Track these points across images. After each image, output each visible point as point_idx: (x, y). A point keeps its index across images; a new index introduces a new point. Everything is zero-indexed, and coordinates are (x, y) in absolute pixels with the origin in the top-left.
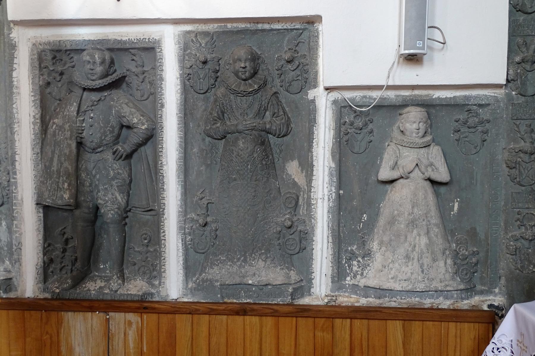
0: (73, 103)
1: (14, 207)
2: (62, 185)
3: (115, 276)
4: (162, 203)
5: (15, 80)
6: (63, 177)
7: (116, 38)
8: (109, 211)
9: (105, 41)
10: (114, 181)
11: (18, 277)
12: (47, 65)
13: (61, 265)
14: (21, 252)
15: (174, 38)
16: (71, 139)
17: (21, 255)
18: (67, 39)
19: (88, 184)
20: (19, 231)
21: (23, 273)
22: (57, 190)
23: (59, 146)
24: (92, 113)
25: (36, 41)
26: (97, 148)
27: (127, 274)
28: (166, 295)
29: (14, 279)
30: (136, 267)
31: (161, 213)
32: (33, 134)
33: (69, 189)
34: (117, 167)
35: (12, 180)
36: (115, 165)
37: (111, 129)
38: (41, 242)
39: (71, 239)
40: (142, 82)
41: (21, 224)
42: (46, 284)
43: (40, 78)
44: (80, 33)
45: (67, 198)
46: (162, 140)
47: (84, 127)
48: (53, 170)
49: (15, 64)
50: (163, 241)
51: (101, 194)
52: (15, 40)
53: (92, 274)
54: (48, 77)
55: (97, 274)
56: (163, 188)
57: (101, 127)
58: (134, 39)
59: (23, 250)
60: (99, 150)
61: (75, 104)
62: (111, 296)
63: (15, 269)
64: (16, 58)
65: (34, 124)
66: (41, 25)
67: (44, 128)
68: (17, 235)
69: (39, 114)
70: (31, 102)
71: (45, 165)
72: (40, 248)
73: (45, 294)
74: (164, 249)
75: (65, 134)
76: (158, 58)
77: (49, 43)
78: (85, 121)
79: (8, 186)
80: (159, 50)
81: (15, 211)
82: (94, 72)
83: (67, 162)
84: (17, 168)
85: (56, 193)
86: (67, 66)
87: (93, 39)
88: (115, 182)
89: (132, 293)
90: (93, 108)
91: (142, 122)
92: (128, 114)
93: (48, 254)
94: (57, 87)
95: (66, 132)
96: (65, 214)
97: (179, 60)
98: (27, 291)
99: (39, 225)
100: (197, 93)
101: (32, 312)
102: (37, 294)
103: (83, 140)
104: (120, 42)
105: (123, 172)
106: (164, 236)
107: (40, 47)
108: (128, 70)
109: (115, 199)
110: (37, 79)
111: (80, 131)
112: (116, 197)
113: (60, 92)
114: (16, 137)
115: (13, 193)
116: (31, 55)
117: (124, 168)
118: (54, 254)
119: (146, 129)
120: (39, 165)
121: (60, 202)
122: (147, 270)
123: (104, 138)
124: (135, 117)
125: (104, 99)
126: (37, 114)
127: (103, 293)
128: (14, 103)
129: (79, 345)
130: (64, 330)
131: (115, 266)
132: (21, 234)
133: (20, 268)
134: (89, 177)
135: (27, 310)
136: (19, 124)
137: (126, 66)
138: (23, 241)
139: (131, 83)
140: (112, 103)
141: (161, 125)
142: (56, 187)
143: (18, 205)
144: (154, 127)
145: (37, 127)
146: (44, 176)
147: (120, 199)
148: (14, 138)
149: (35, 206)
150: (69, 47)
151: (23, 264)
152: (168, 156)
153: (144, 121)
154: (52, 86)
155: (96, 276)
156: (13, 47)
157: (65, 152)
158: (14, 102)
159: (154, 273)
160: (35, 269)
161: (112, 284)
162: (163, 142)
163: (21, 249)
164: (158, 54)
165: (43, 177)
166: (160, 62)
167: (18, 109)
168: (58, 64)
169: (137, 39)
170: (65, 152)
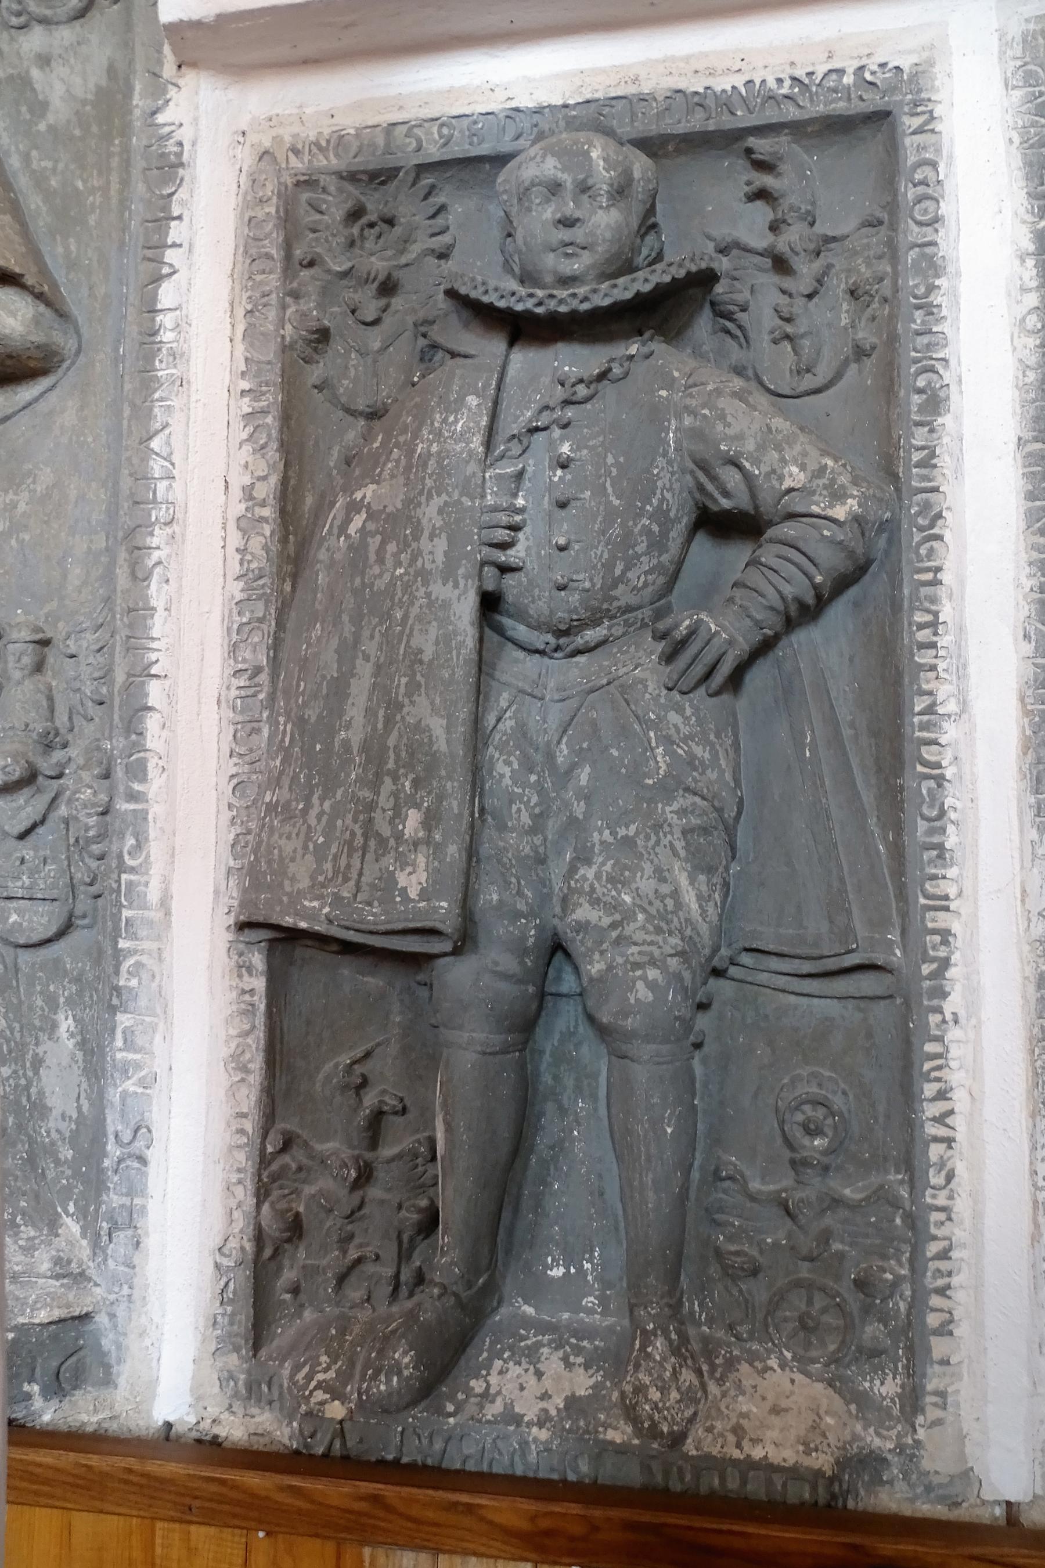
0: (461, 400)
1: (122, 944)
2: (391, 822)
3: (659, 1343)
4: (934, 932)
5: (166, 320)
6: (395, 779)
7: (682, 85)
8: (636, 966)
9: (620, 105)
10: (669, 800)
11: (121, 1311)
13: (345, 1252)
14: (145, 1175)
15: (1002, 53)
17: (143, 1193)
19: (526, 819)
20: (138, 1066)
21: (147, 1286)
22: (365, 849)
24: (562, 439)
25: (277, 139)
26: (584, 624)
27: (699, 1324)
28: (954, 1469)
29: (102, 1319)
30: (759, 1292)
31: (926, 984)
32: (237, 579)
34: (685, 730)
35: (123, 806)
36: (673, 717)
37: (655, 528)
38: (248, 1126)
39: (396, 1113)
40: (810, 296)
41: (154, 1028)
42: (263, 1353)
43: (284, 307)
45: (413, 894)
46: (936, 583)
47: (521, 511)
48: (346, 744)
49: (175, 245)
50: (935, 1151)
51: (598, 876)
52: (177, 136)
53: (504, 1310)
54: (320, 306)
55: (529, 1310)
56: (940, 847)
57: (611, 515)
58: (780, 81)
59: (152, 1169)
60: (591, 635)
61: (472, 400)
62: (646, 1468)
63: (111, 1263)
64: (179, 218)
65: (246, 525)
67: (291, 548)
68: (130, 1086)
69: (274, 480)
70: (237, 424)
71: (301, 722)
72: (241, 1157)
73: (254, 1411)
74: (944, 1193)
76: (912, 160)
77: (339, 141)
78: (527, 484)
79: (102, 836)
80: (916, 122)
81: (127, 964)
82: (578, 234)
84: (149, 745)
85: (356, 862)
86: (415, 250)
87: (560, 102)
88: (675, 806)
89: (776, 1456)
90: (570, 413)
91: (833, 481)
92: (750, 446)
93: (276, 1193)
94: (362, 354)
95: (425, 543)
96: (374, 982)
97: (1028, 164)
98: (162, 1388)
99: (247, 1034)
100: (49, 941)
101: (200, 1533)
102: (213, 1411)
103: (510, 580)
104: (696, 101)
105: (715, 756)
106: (940, 1120)
107: (295, 162)
108: (723, 251)
109: (670, 903)
110: (272, 314)
111: (502, 535)
112: (675, 894)
113: (376, 375)
114: (157, 593)
115: (122, 868)
116: (246, 205)
117: (718, 736)
118: (309, 1190)
119: (857, 520)
120: (258, 731)
121: (374, 915)
122: (824, 1310)
123: (624, 572)
124: (795, 462)
125: (627, 374)
126: (264, 478)
127: (597, 1441)
128: (157, 432)
131: (651, 1280)
132: (148, 1082)
133: (136, 1261)
134: (533, 778)
136: (176, 527)
137: (715, 233)
138: (156, 1117)
139: (744, 309)
140: (663, 393)
141: (927, 506)
142: (359, 832)
143: (143, 933)
144: (888, 515)
145: (256, 544)
146: (295, 778)
147: (694, 906)
148: (146, 598)
149: (230, 936)
150: (434, 152)
151: (152, 1242)
152: (972, 669)
153: (843, 479)
154: (337, 346)
155: (527, 1323)
157: (414, 643)
158: (158, 426)
159: (869, 1329)
160: (210, 1269)
161: (655, 1395)
162: (942, 592)
163: (142, 1160)
164: (908, 141)
165: (286, 782)
166: (924, 183)
167: (175, 458)
168: (369, 245)
169: (794, 79)
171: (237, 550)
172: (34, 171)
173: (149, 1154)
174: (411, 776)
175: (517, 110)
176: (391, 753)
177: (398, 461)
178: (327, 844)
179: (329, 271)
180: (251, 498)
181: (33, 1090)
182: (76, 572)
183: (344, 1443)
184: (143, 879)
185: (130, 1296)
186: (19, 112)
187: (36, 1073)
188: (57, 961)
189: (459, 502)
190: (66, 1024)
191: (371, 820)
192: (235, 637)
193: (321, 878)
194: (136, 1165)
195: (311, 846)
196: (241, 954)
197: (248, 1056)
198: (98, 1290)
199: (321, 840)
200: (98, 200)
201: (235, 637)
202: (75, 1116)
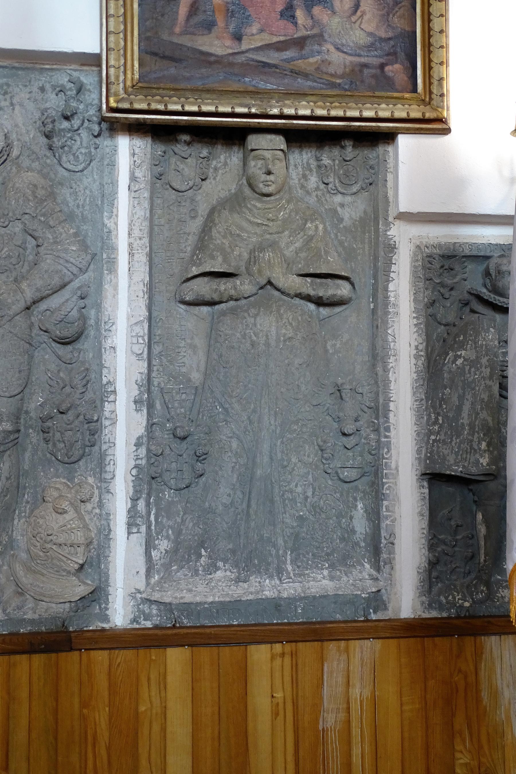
1: (384, 480)
5: (392, 294)
6: (478, 433)
12: (431, 275)
14: (394, 548)
16: (491, 378)
17: (394, 553)
18: (465, 241)
20: (391, 516)
22: (471, 452)
23: (473, 389)
32: (415, 372)
33: (489, 450)
41: (395, 505)
44: (484, 234)
45: (485, 464)
48: (463, 424)
49: (393, 272)
52: (394, 239)
59: (396, 546)
63: (385, 574)
64: (395, 264)
65: (417, 357)
66: (429, 221)
68: (388, 522)
69: (424, 344)
72: (423, 541)
73: (431, 611)
75: (481, 372)
77: (440, 246)
83: (485, 412)
84: (391, 421)
87: (503, 243)
95: (483, 369)
98: (402, 609)
101: (437, 639)
102: (419, 613)
107: (426, 250)
115: (384, 458)
120: (423, 418)
121: (474, 470)
126: (421, 343)
129: (508, 686)
130: (485, 665)
132: (393, 521)
135: (427, 637)
138: (397, 531)
142: (469, 448)
143: (390, 477)
145: (420, 363)
148: (388, 378)
150: (467, 252)
151: (397, 567)
156: (392, 248)
163: (393, 544)
170: (482, 397)
171: (414, 364)
172: (339, 240)
173: (395, 541)
174: (483, 433)
175: (491, 244)
176: (477, 426)
177: (472, 345)
178: (458, 451)
179: (435, 282)
180: (418, 349)
181: (351, 526)
182: (358, 367)
183: (469, 613)
184: (390, 461)
185: (391, 584)
186: (334, 220)
187: (351, 521)
188: (356, 487)
189: (493, 359)
190: (360, 505)
191: (472, 445)
192: (415, 390)
193: (458, 461)
194: (390, 545)
195: (454, 452)
196: (420, 482)
197: (424, 511)
198: (381, 583)
199: (457, 450)
200: (361, 252)
201: (415, 390)
202: (364, 533)
